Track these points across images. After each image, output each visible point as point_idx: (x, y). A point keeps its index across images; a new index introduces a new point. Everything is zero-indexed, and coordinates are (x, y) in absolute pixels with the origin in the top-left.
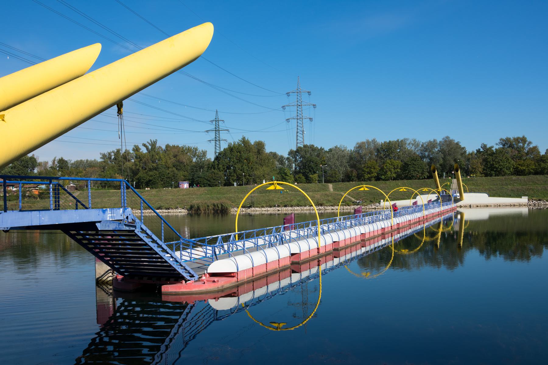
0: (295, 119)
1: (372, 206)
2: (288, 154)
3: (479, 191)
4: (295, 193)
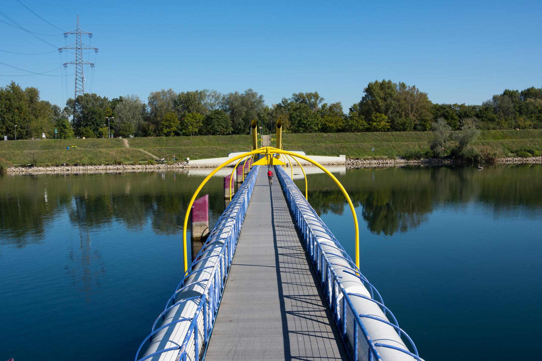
0: (73, 64)
1: (179, 165)
2: (66, 103)
3: (292, 148)
4: (84, 149)
